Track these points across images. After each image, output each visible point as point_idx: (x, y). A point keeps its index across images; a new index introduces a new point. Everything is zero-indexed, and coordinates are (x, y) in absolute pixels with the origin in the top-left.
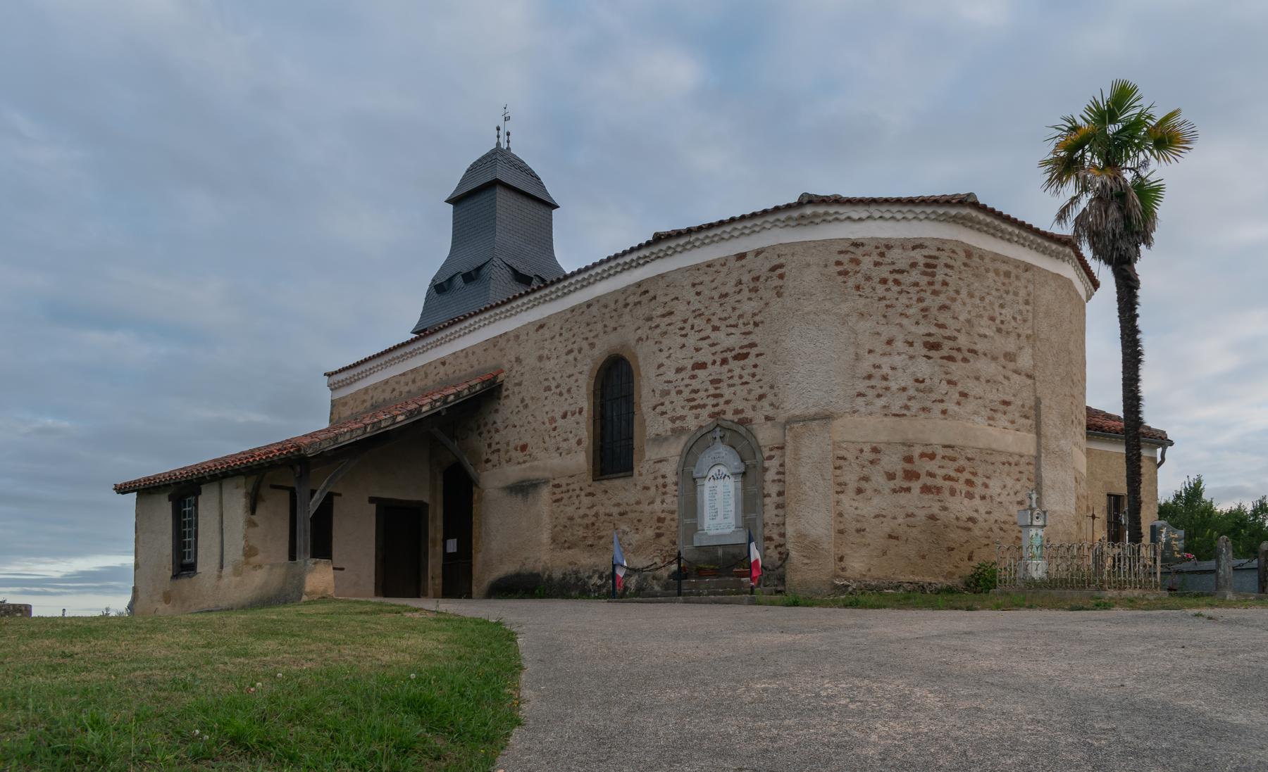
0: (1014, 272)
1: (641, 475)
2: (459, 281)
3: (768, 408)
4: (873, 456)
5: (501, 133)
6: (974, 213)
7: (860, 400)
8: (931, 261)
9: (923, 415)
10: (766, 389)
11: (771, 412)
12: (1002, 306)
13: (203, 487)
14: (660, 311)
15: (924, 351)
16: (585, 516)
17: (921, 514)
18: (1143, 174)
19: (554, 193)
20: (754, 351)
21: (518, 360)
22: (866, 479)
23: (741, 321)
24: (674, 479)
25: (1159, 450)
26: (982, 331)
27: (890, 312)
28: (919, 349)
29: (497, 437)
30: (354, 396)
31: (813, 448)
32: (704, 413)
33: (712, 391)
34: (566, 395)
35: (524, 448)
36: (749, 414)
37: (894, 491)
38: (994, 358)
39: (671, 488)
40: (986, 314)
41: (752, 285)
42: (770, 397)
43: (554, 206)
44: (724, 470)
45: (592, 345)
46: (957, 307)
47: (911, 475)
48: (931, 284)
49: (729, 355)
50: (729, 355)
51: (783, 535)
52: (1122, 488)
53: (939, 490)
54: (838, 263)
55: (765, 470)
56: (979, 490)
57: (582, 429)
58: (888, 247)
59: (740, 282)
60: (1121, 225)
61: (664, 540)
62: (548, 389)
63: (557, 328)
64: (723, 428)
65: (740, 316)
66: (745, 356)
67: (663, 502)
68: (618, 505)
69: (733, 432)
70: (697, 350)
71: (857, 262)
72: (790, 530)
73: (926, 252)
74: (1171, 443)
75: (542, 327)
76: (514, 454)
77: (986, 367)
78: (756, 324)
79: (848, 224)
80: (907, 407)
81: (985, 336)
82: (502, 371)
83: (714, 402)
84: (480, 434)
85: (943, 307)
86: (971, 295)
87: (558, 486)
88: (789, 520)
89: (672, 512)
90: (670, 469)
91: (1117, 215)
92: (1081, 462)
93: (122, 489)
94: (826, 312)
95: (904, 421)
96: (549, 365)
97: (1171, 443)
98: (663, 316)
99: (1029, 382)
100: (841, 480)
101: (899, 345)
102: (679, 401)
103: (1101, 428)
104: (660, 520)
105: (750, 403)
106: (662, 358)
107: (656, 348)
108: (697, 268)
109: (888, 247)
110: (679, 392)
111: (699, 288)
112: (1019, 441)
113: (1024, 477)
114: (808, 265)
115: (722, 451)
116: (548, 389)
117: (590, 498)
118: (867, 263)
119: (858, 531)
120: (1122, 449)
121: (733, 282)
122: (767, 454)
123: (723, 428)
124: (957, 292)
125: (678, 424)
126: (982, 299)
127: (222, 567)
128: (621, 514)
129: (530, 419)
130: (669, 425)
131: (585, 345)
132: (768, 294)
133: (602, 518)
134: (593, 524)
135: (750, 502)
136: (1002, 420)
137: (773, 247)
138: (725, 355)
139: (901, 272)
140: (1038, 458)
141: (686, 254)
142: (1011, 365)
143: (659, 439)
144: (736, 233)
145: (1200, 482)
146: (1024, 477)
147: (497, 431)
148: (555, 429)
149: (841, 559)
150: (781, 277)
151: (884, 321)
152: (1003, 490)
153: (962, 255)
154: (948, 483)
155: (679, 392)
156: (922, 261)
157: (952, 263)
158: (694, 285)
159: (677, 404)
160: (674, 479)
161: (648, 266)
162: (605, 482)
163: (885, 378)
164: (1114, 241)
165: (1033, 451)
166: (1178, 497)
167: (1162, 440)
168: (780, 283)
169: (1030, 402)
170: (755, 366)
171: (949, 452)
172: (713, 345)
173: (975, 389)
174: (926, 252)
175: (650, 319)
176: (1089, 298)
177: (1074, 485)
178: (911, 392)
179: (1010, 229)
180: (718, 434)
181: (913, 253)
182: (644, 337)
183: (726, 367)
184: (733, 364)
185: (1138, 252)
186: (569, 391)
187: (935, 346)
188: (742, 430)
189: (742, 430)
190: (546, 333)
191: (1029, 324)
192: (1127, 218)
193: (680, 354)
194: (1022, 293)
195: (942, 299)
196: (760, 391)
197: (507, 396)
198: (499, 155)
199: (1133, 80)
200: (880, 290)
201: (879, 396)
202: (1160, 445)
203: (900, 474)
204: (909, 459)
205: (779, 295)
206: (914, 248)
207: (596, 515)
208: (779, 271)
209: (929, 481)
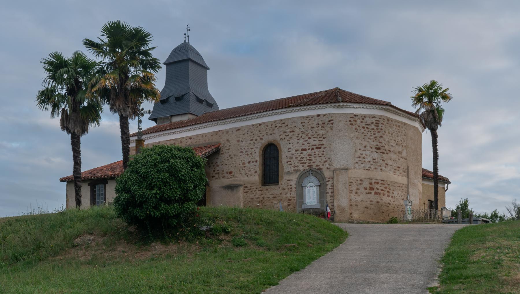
0: (401, 125)
1: (282, 184)
2: (172, 100)
3: (328, 165)
4: (360, 182)
5: (186, 36)
6: (390, 108)
7: (357, 164)
8: (378, 122)
9: (375, 170)
10: (327, 159)
11: (329, 167)
12: (398, 136)
13: (109, 181)
14: (289, 130)
15: (376, 150)
16: (258, 198)
17: (375, 201)
18: (440, 105)
19: (208, 63)
20: (323, 147)
21: (228, 140)
22: (358, 189)
23: (318, 137)
24: (295, 186)
25: (446, 185)
26: (392, 144)
27: (365, 137)
28: (374, 149)
29: (218, 168)
31: (342, 180)
32: (306, 165)
33: (308, 158)
34: (250, 155)
35: (230, 173)
36: (321, 167)
37: (367, 193)
38: (396, 153)
39: (294, 189)
40: (393, 139)
41: (322, 125)
42: (328, 162)
44: (313, 184)
45: (261, 139)
46: (385, 137)
47: (372, 189)
48: (377, 129)
49: (314, 147)
50: (314, 147)
51: (333, 206)
52: (433, 198)
53: (380, 194)
54: (350, 121)
55: (327, 185)
56: (391, 195)
57: (257, 167)
58: (365, 117)
59: (318, 124)
60: (433, 120)
61: (291, 206)
62: (242, 152)
63: (246, 131)
64: (312, 171)
65: (318, 135)
66: (320, 148)
67: (290, 194)
68: (273, 194)
69: (317, 173)
70: (303, 144)
71: (356, 121)
72: (335, 204)
73: (376, 119)
74: (450, 183)
75: (239, 130)
76: (226, 175)
77: (393, 156)
78: (324, 138)
79: (353, 109)
80: (370, 167)
81: (393, 146)
82: (220, 144)
83: (309, 162)
84: (210, 167)
85: (381, 137)
86: (389, 133)
87: (246, 187)
88: (335, 201)
89: (294, 197)
90: (293, 183)
91: (432, 117)
92: (420, 187)
93: (62, 180)
94: (346, 136)
95: (369, 172)
96: (242, 144)
97: (450, 183)
98: (291, 132)
99: (406, 161)
100: (351, 189)
101: (368, 148)
102: (297, 161)
103: (426, 176)
104: (289, 200)
105: (322, 163)
106: (290, 146)
107: (288, 142)
108: (303, 117)
109: (365, 117)
110: (297, 158)
111: (303, 124)
112: (402, 179)
113: (404, 191)
114: (341, 121)
115: (312, 178)
116: (242, 152)
118: (359, 122)
119: (356, 205)
120: (432, 184)
121: (316, 124)
122: (327, 180)
123: (312, 171)
124: (385, 132)
125: (296, 168)
126: (392, 134)
128: (274, 198)
129: (234, 162)
130: (293, 169)
131: (258, 138)
132: (328, 129)
133: (266, 199)
135: (322, 195)
136: (398, 173)
137: (329, 114)
138: (313, 147)
139: (369, 125)
140: (408, 185)
141: (299, 112)
142: (400, 155)
143: (289, 173)
144: (317, 108)
145: (467, 201)
146: (404, 191)
147: (218, 166)
148: (245, 167)
149: (351, 214)
150: (332, 124)
151: (363, 140)
152: (398, 194)
153: (386, 120)
154: (382, 192)
155: (297, 158)
156: (375, 122)
157: (383, 123)
158: (302, 123)
159: (296, 162)
160: (295, 186)
162: (267, 186)
163: (364, 158)
164: (431, 124)
165: (406, 183)
166: (458, 208)
167: (446, 181)
168: (332, 126)
169: (406, 167)
170: (323, 151)
171: (383, 182)
172: (309, 143)
173: (390, 162)
174: (376, 119)
175: (285, 132)
176: (423, 132)
177: (418, 195)
178: (372, 163)
179: (400, 112)
180: (311, 172)
181: (372, 119)
183: (313, 151)
184: (315, 150)
185: (437, 128)
186: (251, 154)
187: (378, 149)
188: (319, 172)
189: (319, 172)
190: (241, 132)
191: (405, 142)
192: (434, 118)
193: (297, 145)
194: (403, 132)
195: (381, 134)
196: (325, 160)
197: (223, 153)
199: (436, 80)
200: (363, 130)
201: (362, 163)
202: (446, 183)
203: (368, 188)
204: (371, 184)
205: (331, 129)
206: (373, 118)
207: (263, 198)
208: (331, 122)
209: (377, 191)
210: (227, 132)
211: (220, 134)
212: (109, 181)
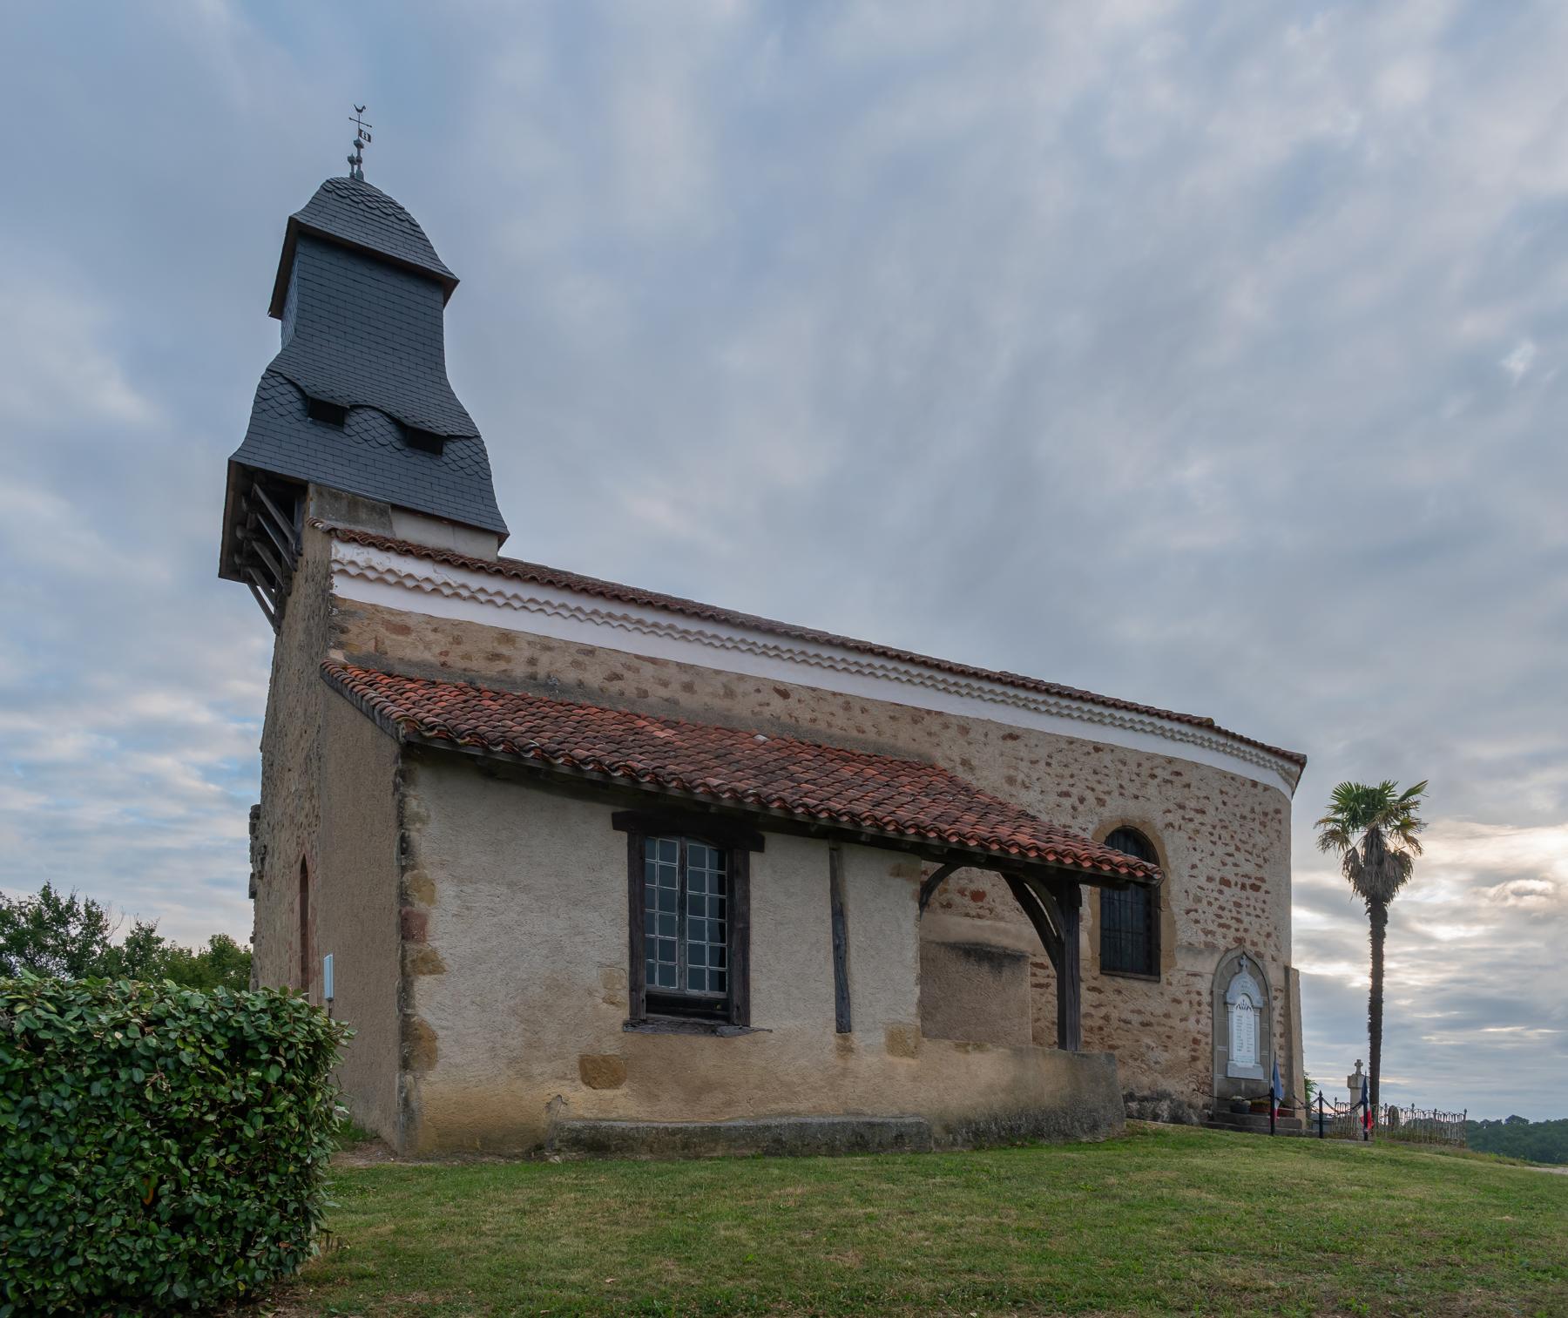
30: (437, 625)
33: (1234, 914)
61: (1200, 1065)
63: (1042, 753)
67: (1198, 1021)
89: (1206, 1035)
90: (1204, 985)
110: (1210, 904)
117: (1095, 994)
127: (843, 1025)
133: (1115, 1023)
134: (1101, 1028)
161: (1180, 745)
162: (1120, 980)
182: (1176, 824)
198: (347, 192)
207: (1106, 1018)
210: (964, 730)
212: (773, 841)
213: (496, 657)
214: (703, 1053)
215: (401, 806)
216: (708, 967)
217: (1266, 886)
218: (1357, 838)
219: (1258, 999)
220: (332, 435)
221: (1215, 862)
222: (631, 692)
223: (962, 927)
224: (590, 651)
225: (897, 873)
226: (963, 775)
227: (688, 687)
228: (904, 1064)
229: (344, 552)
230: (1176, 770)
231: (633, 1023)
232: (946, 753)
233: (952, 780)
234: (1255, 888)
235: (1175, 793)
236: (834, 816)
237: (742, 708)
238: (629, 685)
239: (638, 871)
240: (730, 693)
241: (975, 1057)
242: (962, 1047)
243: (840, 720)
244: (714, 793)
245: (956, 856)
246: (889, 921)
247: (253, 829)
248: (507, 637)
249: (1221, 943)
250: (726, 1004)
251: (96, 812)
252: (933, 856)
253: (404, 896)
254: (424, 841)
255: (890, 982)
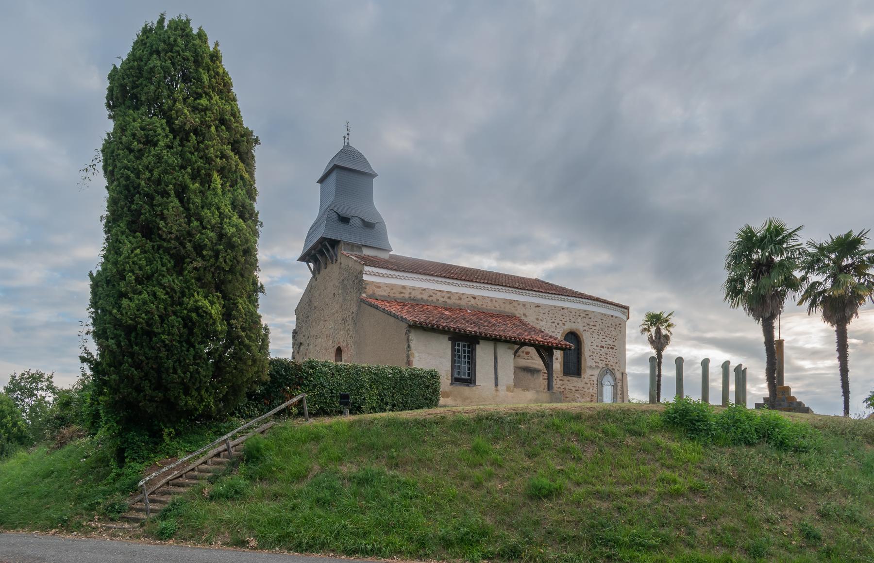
13: (481, 342)
30: (387, 285)
43: (373, 175)
63: (547, 311)
69: (609, 370)
127: (496, 385)
198: (347, 152)
210: (524, 305)
211: (515, 304)
212: (481, 342)
213: (401, 293)
214: (466, 390)
215: (408, 338)
216: (467, 371)
217: (616, 346)
218: (653, 329)
219: (612, 383)
220: (346, 226)
221: (599, 341)
222: (435, 300)
223: (523, 362)
224: (424, 290)
225: (509, 348)
226: (523, 318)
227: (449, 298)
228: (510, 394)
229: (366, 268)
230: (587, 314)
231: (452, 384)
232: (519, 312)
233: (521, 321)
234: (612, 348)
235: (586, 320)
236: (496, 336)
237: (463, 303)
238: (434, 298)
239: (453, 350)
240: (460, 299)
241: (527, 393)
242: (524, 390)
243: (490, 304)
244: (470, 332)
245: (523, 344)
246: (507, 359)
247: (294, 337)
248: (404, 287)
249: (601, 366)
250: (470, 380)
251: (42, 316)
252: (517, 344)
253: (408, 356)
254: (412, 344)
255: (507, 375)
